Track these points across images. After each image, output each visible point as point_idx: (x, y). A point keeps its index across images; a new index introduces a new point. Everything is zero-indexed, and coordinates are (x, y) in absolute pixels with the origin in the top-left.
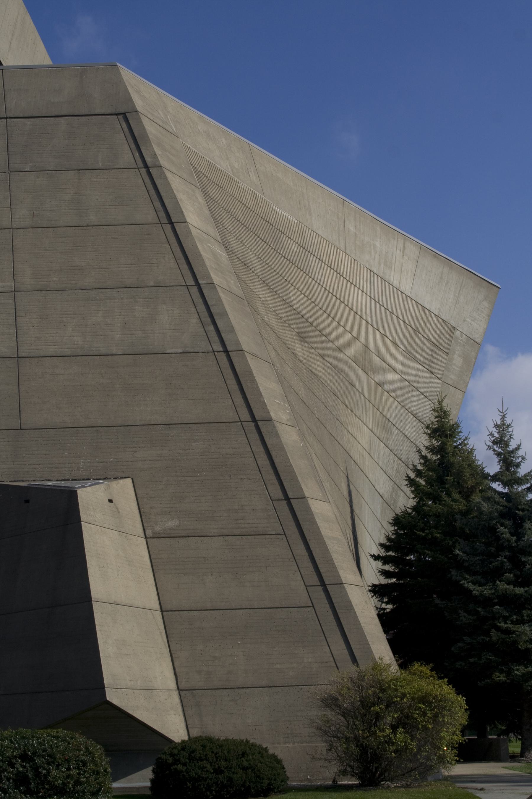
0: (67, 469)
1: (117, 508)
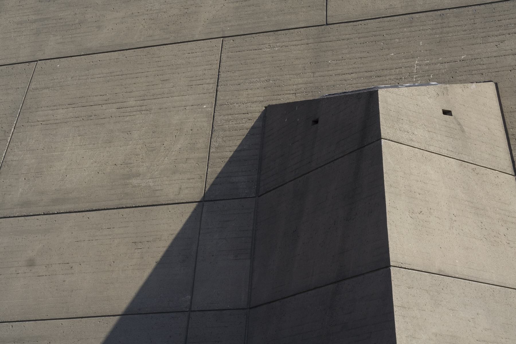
0: (392, 77)
1: (459, 124)
